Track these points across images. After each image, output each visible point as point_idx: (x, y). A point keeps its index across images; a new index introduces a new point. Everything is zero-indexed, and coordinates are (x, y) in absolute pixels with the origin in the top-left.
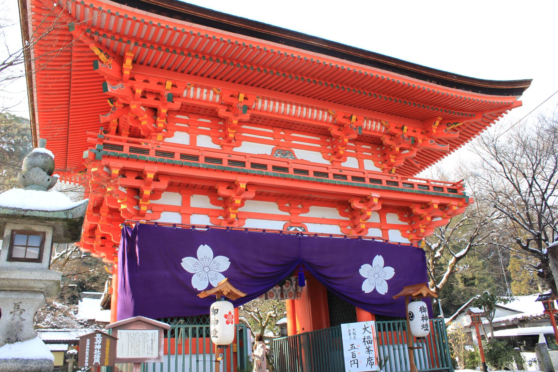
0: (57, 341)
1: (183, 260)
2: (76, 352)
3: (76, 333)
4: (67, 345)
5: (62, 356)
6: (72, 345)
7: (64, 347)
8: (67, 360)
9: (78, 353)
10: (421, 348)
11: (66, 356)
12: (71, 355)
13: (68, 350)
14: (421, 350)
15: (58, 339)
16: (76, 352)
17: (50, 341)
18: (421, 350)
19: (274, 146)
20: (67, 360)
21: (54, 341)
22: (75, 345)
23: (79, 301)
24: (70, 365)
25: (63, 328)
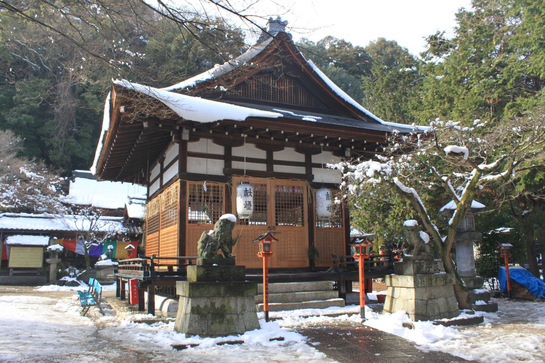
0: (32, 230)
1: (285, 148)
2: (61, 248)
3: (62, 220)
4: (47, 238)
5: (40, 252)
6: (55, 238)
7: (44, 240)
8: (48, 260)
9: (64, 249)
10: (270, 168)
11: (47, 254)
12: (54, 252)
13: (49, 245)
14: (262, 167)
15: (35, 228)
16: (61, 248)
17: (22, 230)
18: (262, 167)
19: (178, 161)
20: (48, 260)
21: (27, 230)
22: (59, 238)
23: (71, 181)
24: (53, 268)
25: (43, 212)
